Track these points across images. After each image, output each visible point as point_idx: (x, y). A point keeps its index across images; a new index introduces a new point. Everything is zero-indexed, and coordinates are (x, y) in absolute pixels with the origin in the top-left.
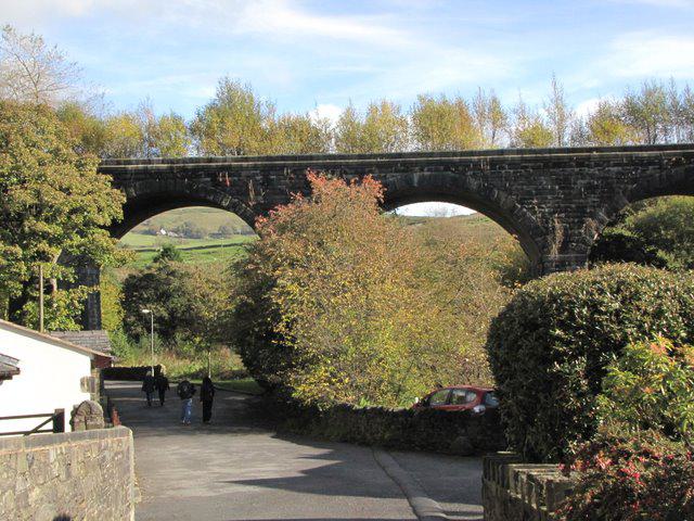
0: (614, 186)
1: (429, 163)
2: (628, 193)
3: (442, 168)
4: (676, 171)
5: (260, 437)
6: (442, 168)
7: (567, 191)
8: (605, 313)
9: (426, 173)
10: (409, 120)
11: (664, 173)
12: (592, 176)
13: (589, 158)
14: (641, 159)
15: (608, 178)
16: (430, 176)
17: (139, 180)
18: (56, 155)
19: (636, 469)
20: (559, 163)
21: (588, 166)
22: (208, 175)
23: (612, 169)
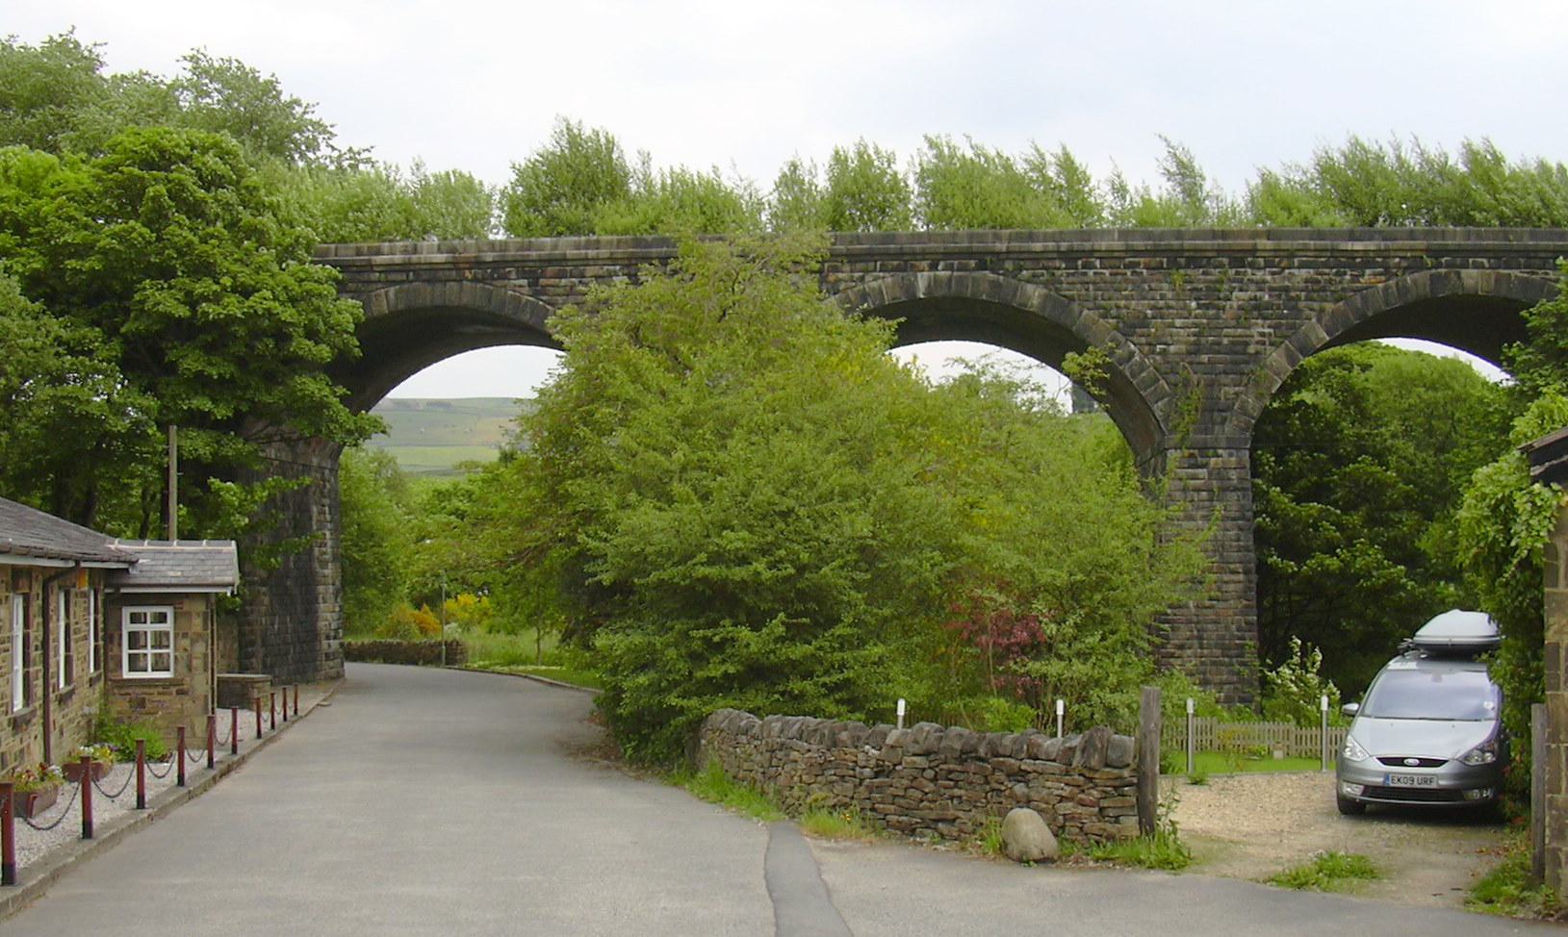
0: (1302, 304)
1: (948, 255)
2: (1326, 318)
3: (972, 263)
4: (1415, 282)
5: (640, 788)
6: (972, 263)
7: (1211, 312)
8: (985, 533)
9: (943, 274)
10: (913, 185)
11: (1392, 282)
12: (1260, 285)
13: (1253, 251)
14: (1351, 255)
15: (1287, 290)
16: (950, 279)
17: (394, 283)
18: (528, 226)
19: (184, 512)
20: (1196, 259)
21: (1252, 266)
22: (521, 275)
23: (1295, 271)
